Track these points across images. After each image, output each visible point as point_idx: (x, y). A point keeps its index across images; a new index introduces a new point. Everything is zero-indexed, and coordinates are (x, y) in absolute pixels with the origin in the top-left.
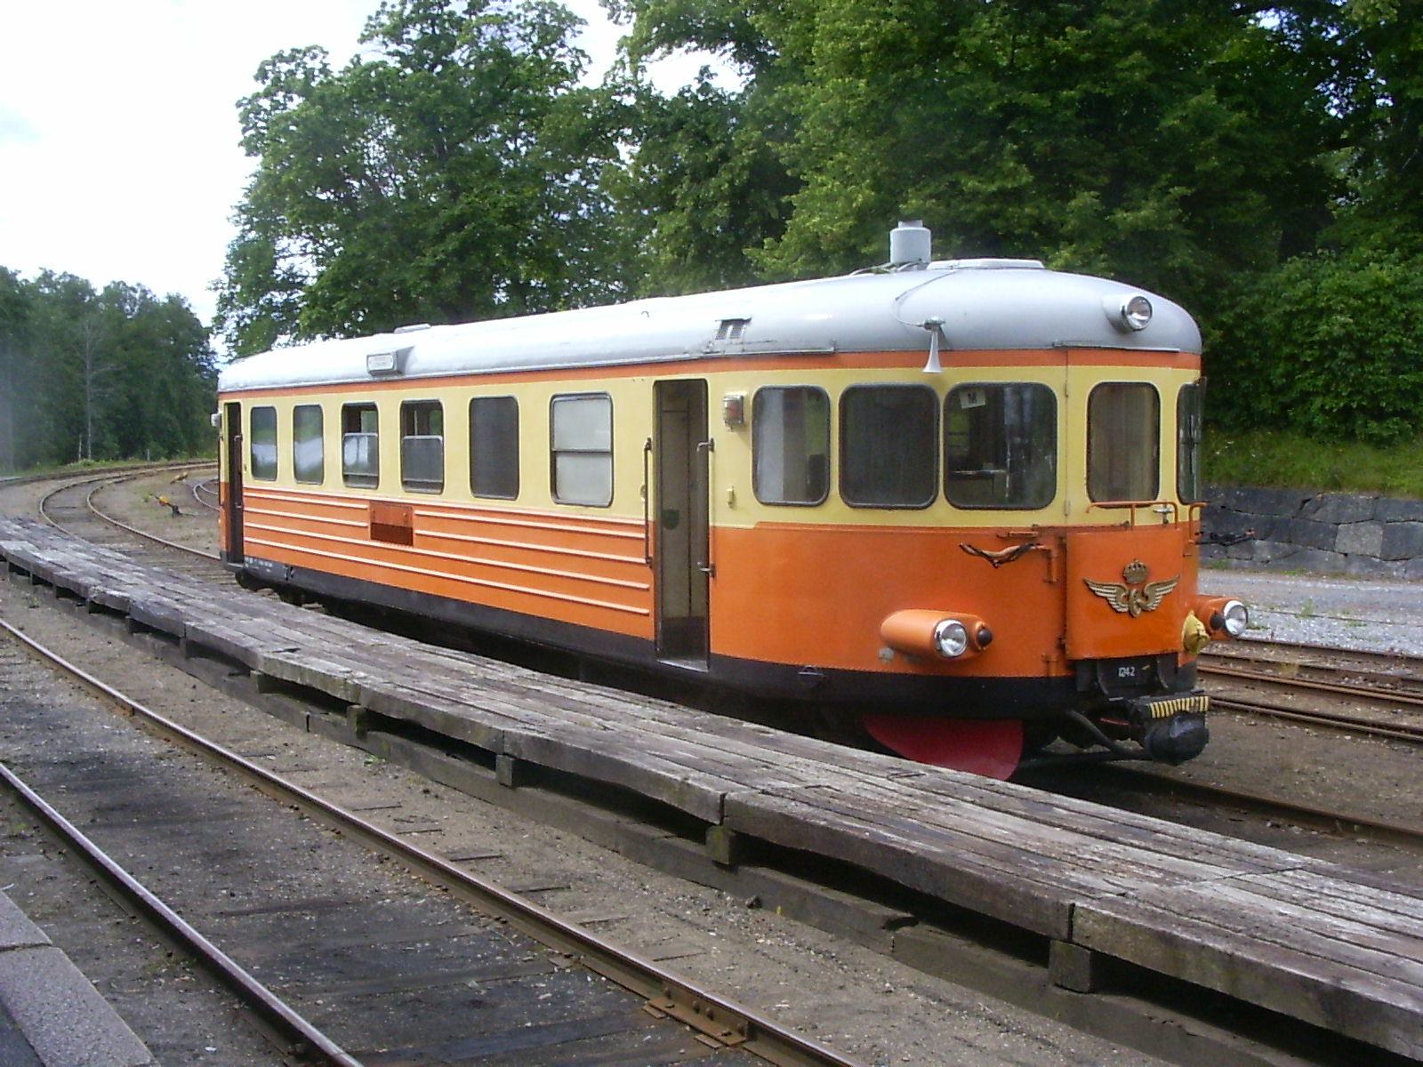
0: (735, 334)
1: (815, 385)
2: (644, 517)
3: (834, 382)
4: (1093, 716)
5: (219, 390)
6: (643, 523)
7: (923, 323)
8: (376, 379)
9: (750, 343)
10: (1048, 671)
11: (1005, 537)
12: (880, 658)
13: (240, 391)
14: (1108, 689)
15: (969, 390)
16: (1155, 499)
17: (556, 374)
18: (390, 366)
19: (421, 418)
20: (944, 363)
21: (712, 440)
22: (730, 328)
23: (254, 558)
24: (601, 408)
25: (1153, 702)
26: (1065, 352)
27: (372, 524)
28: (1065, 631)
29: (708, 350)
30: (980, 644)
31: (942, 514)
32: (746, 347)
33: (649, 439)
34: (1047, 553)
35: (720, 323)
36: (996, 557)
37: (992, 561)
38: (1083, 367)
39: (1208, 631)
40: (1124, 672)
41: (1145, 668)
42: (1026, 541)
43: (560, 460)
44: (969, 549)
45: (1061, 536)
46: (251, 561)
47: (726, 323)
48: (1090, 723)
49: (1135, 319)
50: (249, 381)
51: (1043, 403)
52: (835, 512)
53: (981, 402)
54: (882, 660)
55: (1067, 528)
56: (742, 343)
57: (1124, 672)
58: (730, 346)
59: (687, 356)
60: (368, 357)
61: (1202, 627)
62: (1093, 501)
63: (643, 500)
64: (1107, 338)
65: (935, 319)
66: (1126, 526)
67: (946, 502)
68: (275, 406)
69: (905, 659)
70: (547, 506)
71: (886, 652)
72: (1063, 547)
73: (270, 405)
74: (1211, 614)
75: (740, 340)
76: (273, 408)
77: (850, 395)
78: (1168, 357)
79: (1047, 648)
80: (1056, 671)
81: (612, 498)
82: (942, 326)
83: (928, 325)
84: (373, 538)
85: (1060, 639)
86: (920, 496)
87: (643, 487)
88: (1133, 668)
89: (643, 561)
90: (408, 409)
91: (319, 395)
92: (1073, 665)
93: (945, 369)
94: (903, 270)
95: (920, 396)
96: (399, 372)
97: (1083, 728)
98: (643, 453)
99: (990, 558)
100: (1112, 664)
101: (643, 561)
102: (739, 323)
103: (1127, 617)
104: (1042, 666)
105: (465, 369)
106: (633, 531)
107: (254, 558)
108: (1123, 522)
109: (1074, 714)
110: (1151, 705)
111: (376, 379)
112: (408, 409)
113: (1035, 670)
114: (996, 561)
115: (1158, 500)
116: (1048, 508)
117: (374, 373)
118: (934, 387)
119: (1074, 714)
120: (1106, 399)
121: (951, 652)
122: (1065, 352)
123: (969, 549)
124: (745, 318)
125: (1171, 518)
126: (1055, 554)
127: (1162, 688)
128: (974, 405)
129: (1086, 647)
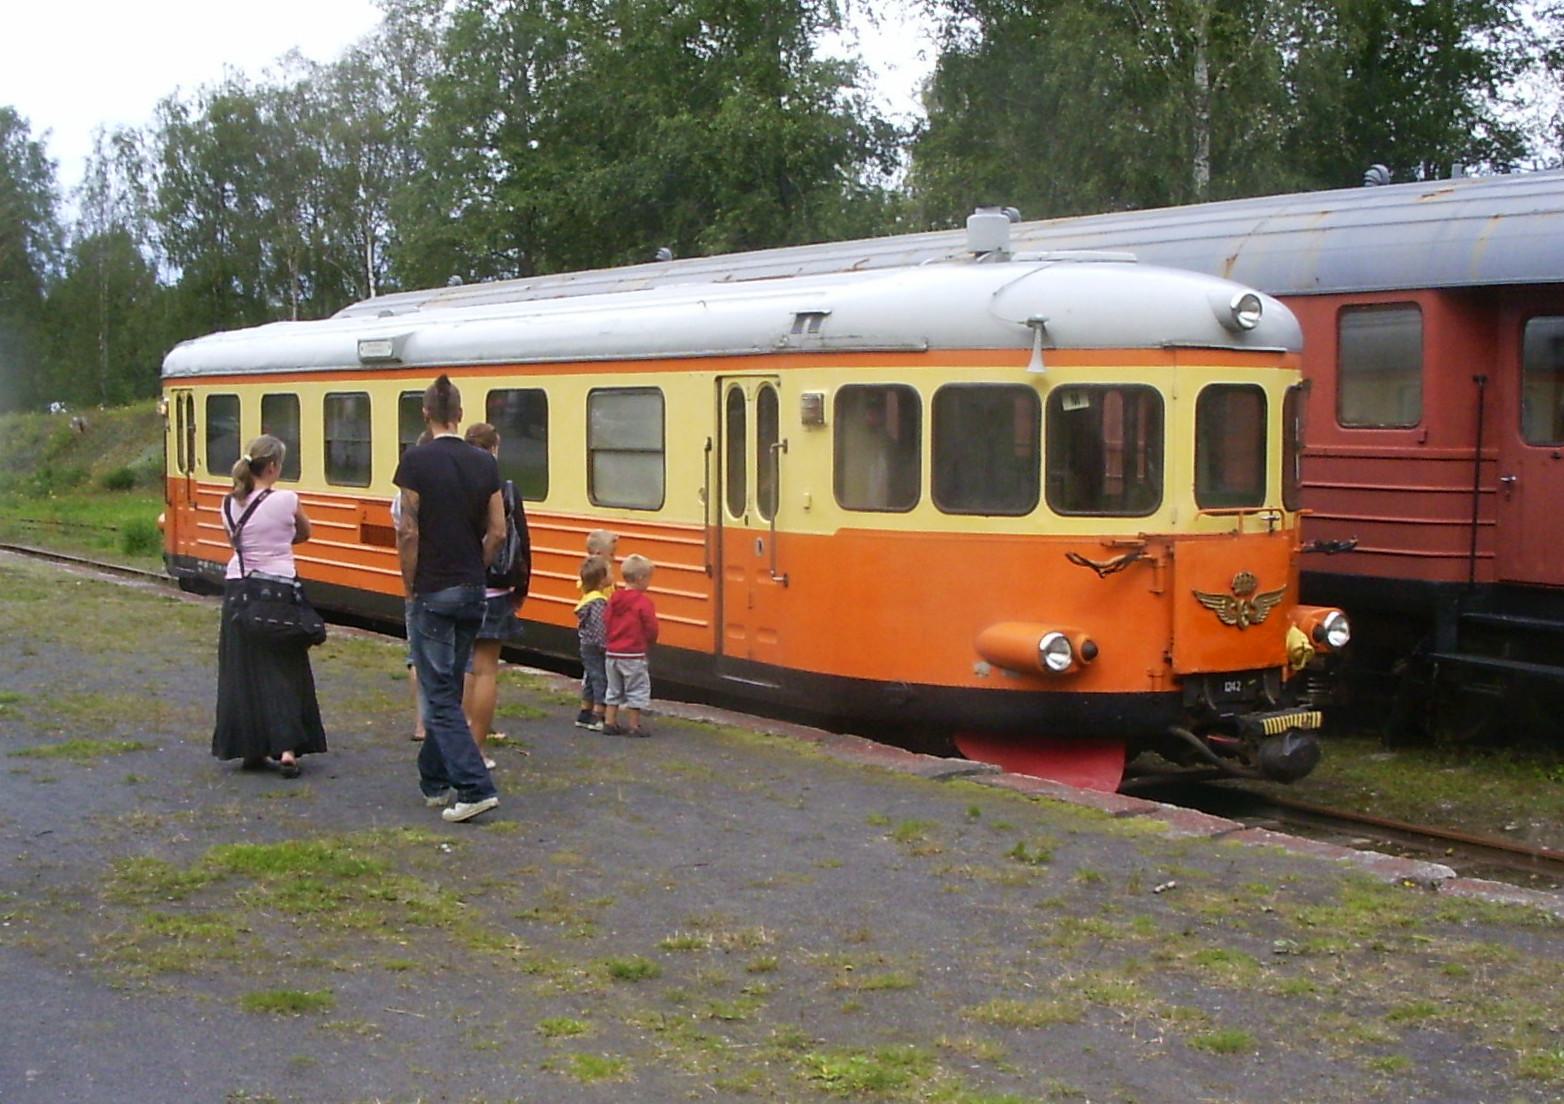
0: (814, 327)
1: (1149, 383)
2: (704, 522)
3: (926, 382)
4: (1200, 732)
5: (164, 376)
6: (703, 528)
7: (1026, 319)
8: (368, 367)
9: (831, 338)
10: (1153, 687)
11: (1113, 546)
12: (977, 673)
13: (192, 377)
14: (1216, 704)
15: (1074, 391)
16: (1262, 505)
17: (847, 358)
18: (387, 352)
19: (280, 411)
20: (1047, 363)
21: (786, 441)
22: (808, 321)
23: (210, 562)
24: (653, 402)
25: (1266, 717)
26: (1174, 351)
27: (363, 525)
28: (1172, 644)
29: (782, 345)
30: (1086, 659)
31: (1043, 521)
32: (827, 341)
33: (709, 439)
34: (1153, 561)
35: (794, 316)
36: (1102, 567)
37: (1098, 571)
38: (1185, 367)
39: (1310, 643)
40: (1230, 687)
41: (1251, 683)
42: (1133, 553)
43: (600, 461)
44: (1076, 559)
45: (1166, 542)
46: (206, 565)
47: (801, 317)
48: (1197, 741)
49: (1246, 318)
50: (204, 366)
51: (1145, 406)
52: (926, 517)
53: (1084, 404)
54: (978, 674)
55: (1173, 536)
56: (822, 338)
57: (1230, 687)
58: (805, 340)
59: (756, 350)
60: (359, 342)
61: (1306, 640)
62: (1200, 508)
63: (703, 504)
64: (1216, 337)
65: (1039, 316)
66: (1234, 534)
67: (1047, 508)
68: (660, 386)
69: (1003, 673)
70: (582, 508)
71: (983, 666)
72: (1170, 556)
73: (292, 392)
74: (1313, 626)
75: (819, 336)
76: (236, 397)
77: (945, 396)
78: (1275, 356)
79: (1159, 668)
80: (1163, 686)
81: (663, 501)
82: (1046, 324)
83: (1032, 323)
84: (364, 541)
85: (1166, 652)
86: (1023, 505)
87: (701, 490)
88: (1239, 683)
89: (703, 569)
90: (268, 402)
91: (542, 377)
92: (1179, 679)
93: (1048, 368)
94: (981, 262)
95: (1027, 393)
96: (1344, 310)
97: (1184, 743)
98: (704, 453)
99: (1096, 568)
100: (1217, 679)
101: (703, 569)
102: (818, 316)
103: (1235, 629)
104: (1148, 680)
105: (480, 358)
106: (693, 538)
107: (210, 562)
108: (1231, 530)
109: (1180, 731)
110: (1265, 721)
111: (368, 367)
112: (268, 402)
113: (1140, 685)
114: (1102, 570)
115: (1265, 507)
116: (1155, 515)
117: (366, 361)
118: (1035, 387)
119: (1180, 731)
120: (1212, 401)
121: (1056, 667)
122: (1174, 351)
123: (1076, 559)
124: (826, 311)
125: (1278, 526)
126: (1161, 563)
127: (1270, 704)
128: (1077, 407)
129: (1189, 663)
